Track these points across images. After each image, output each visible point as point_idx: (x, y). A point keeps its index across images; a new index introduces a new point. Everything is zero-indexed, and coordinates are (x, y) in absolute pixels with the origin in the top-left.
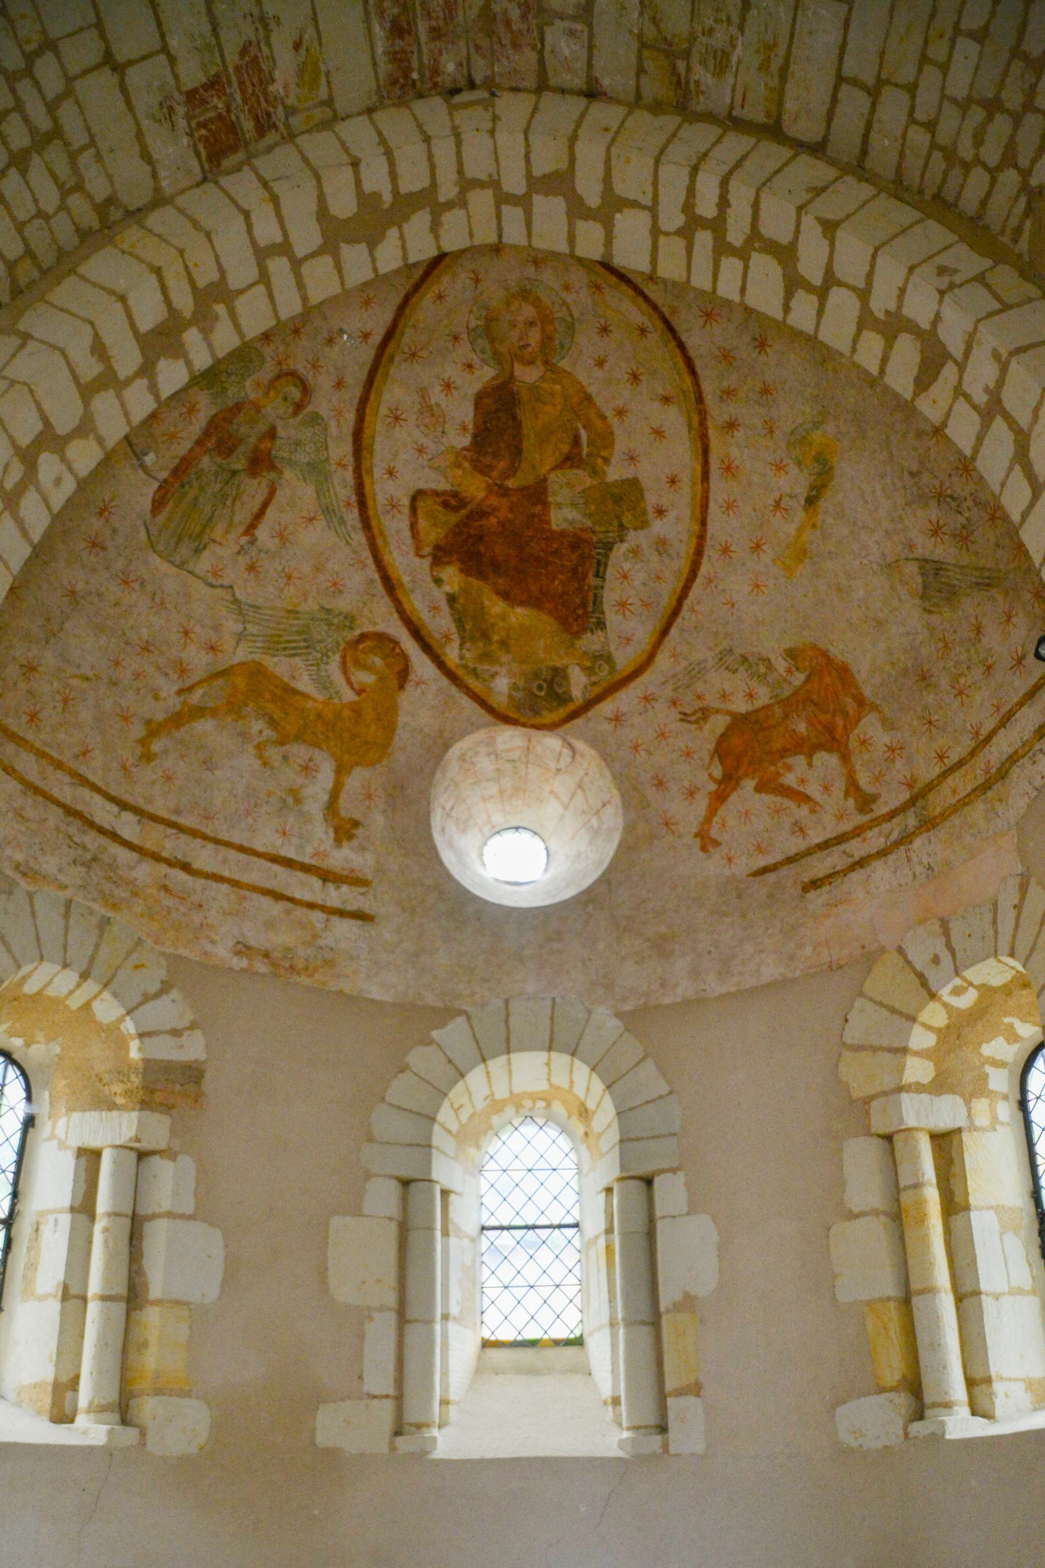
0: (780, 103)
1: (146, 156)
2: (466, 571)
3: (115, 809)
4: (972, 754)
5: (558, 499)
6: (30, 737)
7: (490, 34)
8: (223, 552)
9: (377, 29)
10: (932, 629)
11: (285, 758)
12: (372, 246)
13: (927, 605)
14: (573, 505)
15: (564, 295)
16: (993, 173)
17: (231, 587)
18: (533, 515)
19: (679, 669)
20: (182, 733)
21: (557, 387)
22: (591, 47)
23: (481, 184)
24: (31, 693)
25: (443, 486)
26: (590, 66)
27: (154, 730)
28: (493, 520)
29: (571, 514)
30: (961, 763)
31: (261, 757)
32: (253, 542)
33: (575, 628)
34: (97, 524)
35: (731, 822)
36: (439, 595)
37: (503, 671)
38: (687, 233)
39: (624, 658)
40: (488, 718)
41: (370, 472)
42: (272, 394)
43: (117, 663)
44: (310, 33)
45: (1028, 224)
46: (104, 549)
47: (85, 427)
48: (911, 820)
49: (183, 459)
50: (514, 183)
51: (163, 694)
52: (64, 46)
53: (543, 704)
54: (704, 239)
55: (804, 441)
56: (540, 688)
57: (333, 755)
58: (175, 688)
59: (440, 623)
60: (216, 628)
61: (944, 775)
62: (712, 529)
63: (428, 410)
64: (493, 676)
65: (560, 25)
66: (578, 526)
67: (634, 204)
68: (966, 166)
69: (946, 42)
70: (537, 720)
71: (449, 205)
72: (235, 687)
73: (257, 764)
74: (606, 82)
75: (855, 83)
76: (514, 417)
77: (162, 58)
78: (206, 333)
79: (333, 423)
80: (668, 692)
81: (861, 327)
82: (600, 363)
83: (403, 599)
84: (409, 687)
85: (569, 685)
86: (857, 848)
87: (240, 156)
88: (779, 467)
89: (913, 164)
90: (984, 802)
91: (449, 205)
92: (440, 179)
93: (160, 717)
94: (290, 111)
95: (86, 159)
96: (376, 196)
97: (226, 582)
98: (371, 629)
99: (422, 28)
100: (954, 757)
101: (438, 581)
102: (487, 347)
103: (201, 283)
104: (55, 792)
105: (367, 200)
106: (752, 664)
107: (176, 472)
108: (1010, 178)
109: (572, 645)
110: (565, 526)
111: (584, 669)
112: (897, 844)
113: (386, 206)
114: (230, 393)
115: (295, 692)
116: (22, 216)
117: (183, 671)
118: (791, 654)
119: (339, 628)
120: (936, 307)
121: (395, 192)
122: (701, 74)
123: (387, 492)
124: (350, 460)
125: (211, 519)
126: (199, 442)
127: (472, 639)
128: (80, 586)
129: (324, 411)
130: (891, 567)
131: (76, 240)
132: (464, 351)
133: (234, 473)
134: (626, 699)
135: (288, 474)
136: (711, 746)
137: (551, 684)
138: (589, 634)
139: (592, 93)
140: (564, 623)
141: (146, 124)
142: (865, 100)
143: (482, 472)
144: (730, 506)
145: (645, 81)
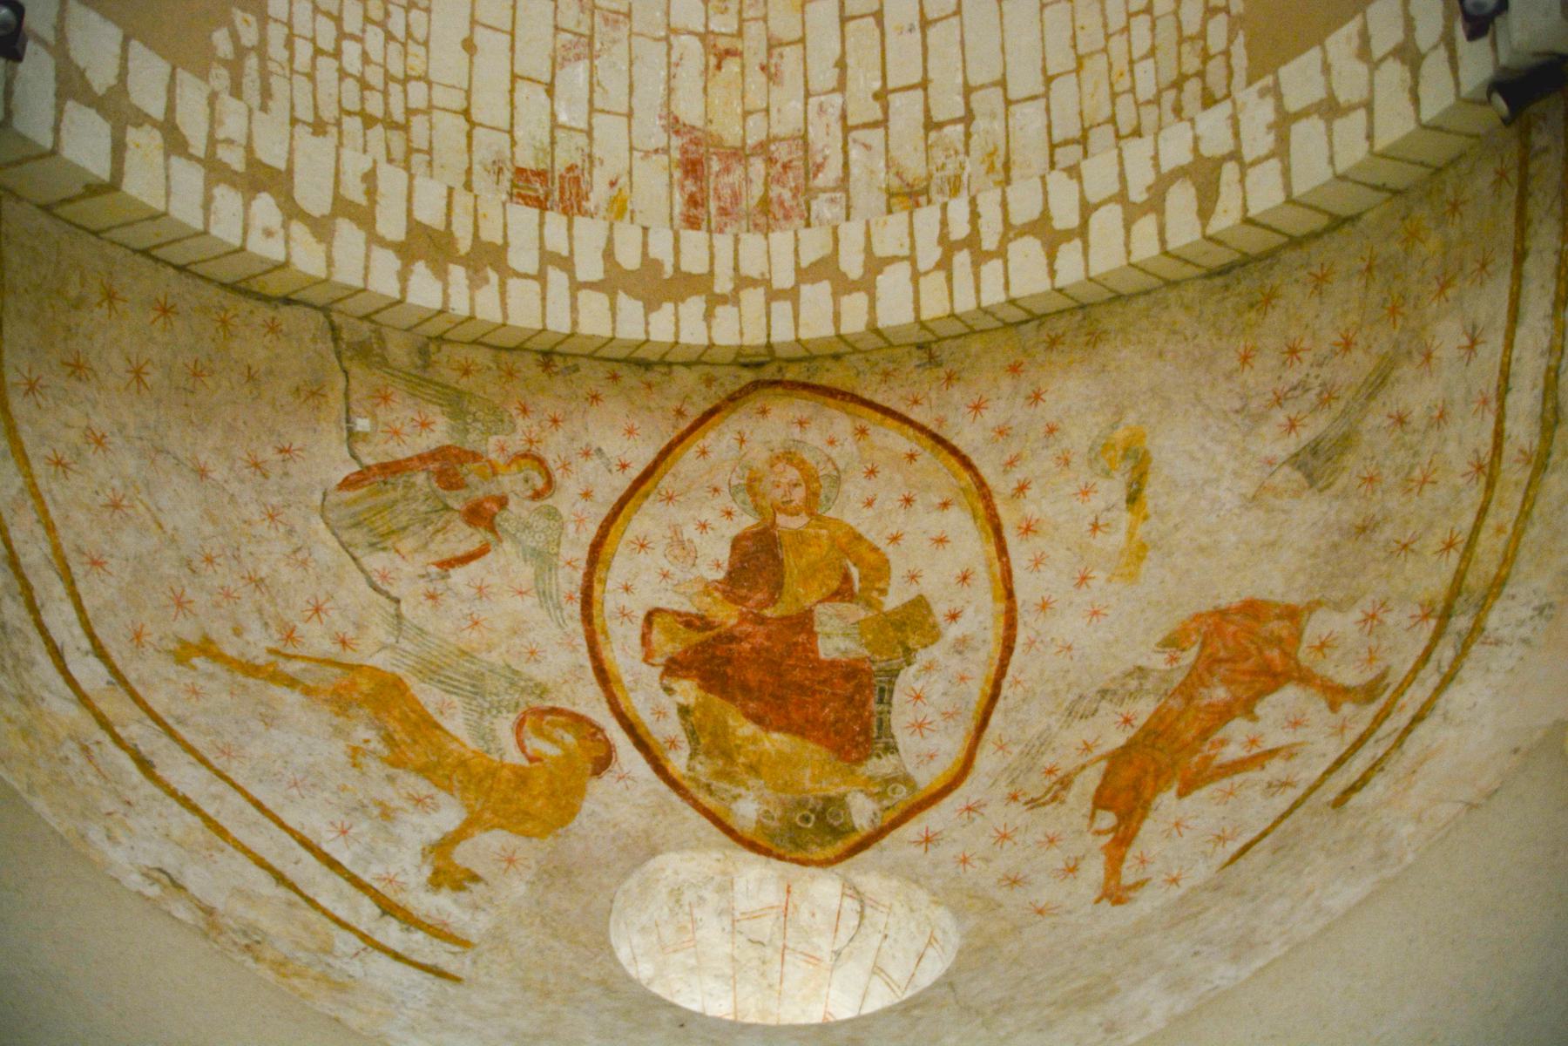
5: (827, 629)
8: (405, 567)
13: (1320, 484)
14: (846, 635)
15: (828, 450)
17: (398, 601)
18: (795, 644)
21: (824, 532)
23: (754, 283)
25: (687, 607)
27: (207, 648)
28: (747, 646)
29: (843, 644)
32: (445, 577)
34: (269, 455)
36: (669, 704)
37: (751, 795)
38: (945, 264)
39: (927, 777)
41: (603, 581)
42: (514, 468)
44: (624, 180)
46: (265, 476)
49: (398, 463)
50: (784, 278)
56: (806, 819)
58: (272, 645)
62: (1020, 596)
63: (679, 545)
64: (735, 798)
65: (823, 196)
66: (852, 656)
69: (1127, 77)
70: (799, 855)
71: (723, 300)
76: (775, 557)
82: (870, 503)
83: (619, 694)
84: (607, 777)
88: (1085, 492)
92: (717, 270)
96: (658, 264)
97: (394, 592)
99: (713, 206)
102: (749, 500)
107: (384, 467)
109: (853, 772)
110: (835, 655)
113: (666, 276)
121: (677, 267)
125: (404, 529)
126: (421, 458)
127: (708, 754)
129: (564, 510)
132: (724, 500)
133: (447, 508)
135: (507, 545)
137: (821, 816)
138: (875, 759)
140: (841, 752)
141: (477, 168)
143: (735, 602)
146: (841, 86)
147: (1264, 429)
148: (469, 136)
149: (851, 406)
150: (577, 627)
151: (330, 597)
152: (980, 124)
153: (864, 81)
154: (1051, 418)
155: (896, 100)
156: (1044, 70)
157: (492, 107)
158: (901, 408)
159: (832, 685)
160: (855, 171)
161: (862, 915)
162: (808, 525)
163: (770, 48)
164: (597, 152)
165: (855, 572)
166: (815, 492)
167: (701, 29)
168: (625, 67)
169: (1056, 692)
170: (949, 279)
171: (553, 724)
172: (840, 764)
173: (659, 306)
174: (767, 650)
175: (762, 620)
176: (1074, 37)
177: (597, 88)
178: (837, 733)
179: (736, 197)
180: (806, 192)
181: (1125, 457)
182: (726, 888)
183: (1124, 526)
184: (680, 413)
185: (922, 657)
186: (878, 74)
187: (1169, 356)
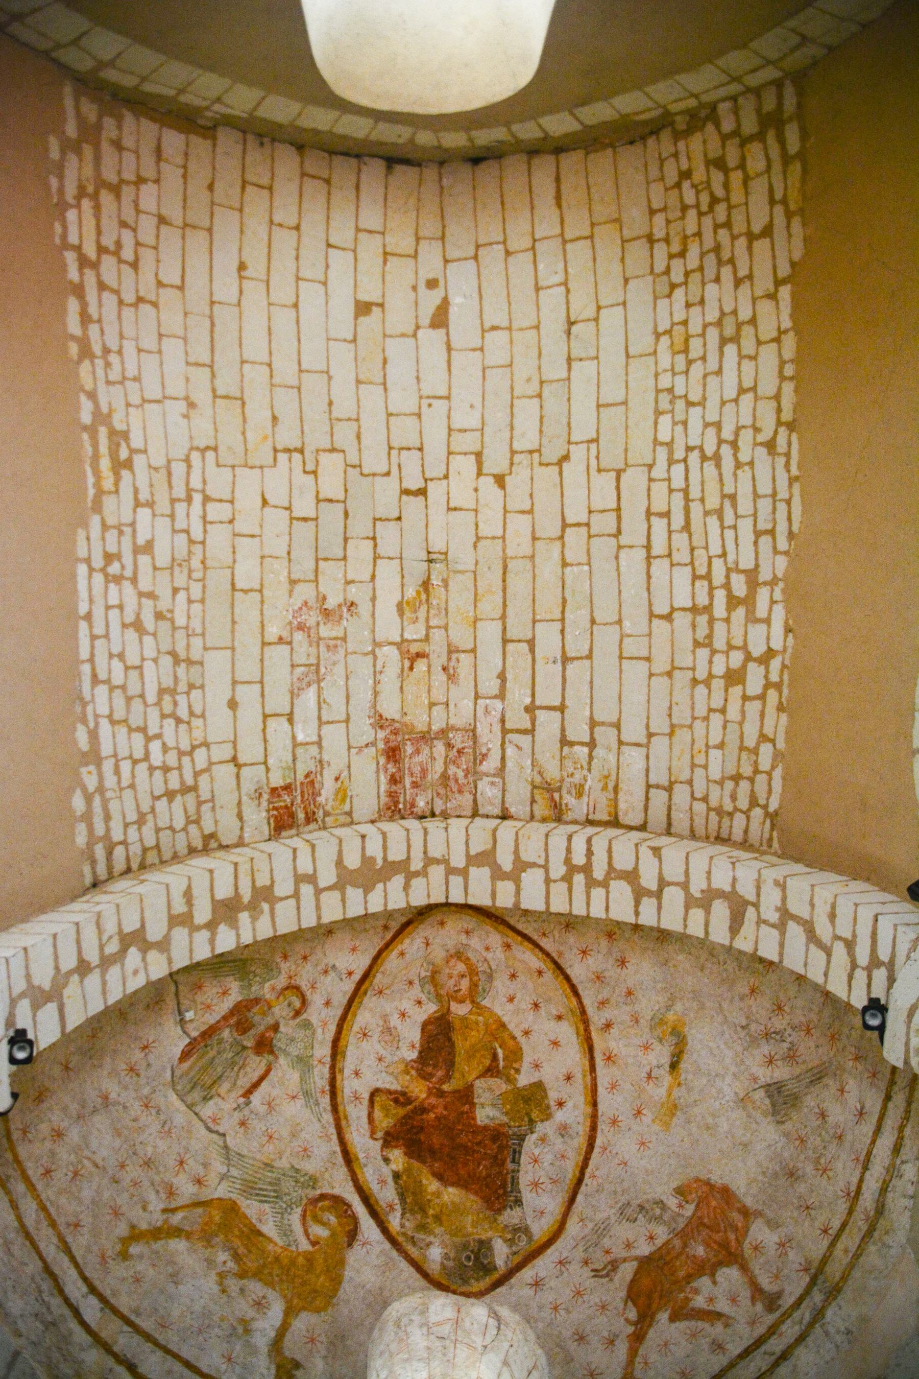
0: (616, 807)
1: (240, 816)
2: (408, 1154)
3: (85, 1289)
4: (850, 1212)
6: (39, 1187)
7: (446, 787)
8: (222, 1107)
9: (382, 777)
10: (787, 1135)
11: (242, 1290)
12: (366, 893)
14: (494, 1105)
15: (485, 954)
16: (747, 813)
17: (224, 1135)
19: (587, 1231)
20: (158, 1245)
22: (504, 791)
23: (437, 861)
24: (53, 1154)
25: (395, 1086)
26: (503, 802)
27: (135, 1235)
28: (432, 1115)
29: (491, 1112)
30: (844, 1225)
31: (221, 1284)
32: (248, 1103)
33: (497, 1206)
34: (138, 1055)
35: (653, 1357)
36: (387, 1172)
37: (436, 1241)
38: (567, 878)
39: (540, 1229)
40: (423, 1283)
41: (342, 1071)
43: (123, 1166)
44: (345, 774)
45: (775, 834)
46: (138, 1075)
47: (163, 945)
48: (817, 1297)
49: (211, 1027)
50: (458, 861)
51: (151, 1208)
52: (213, 747)
53: (471, 1274)
54: (579, 879)
55: (662, 1022)
56: (468, 1258)
57: (285, 1297)
58: (162, 1206)
59: (387, 1195)
60: (206, 1165)
61: (833, 1244)
62: (601, 1108)
65: (486, 780)
67: (534, 865)
68: (731, 815)
69: (703, 754)
71: (417, 874)
72: (211, 1217)
73: (216, 1289)
74: (512, 810)
75: (657, 787)
76: (450, 1039)
77: (263, 767)
78: (254, 919)
79: (319, 1031)
80: (579, 1254)
81: (687, 908)
82: (511, 999)
83: (358, 1171)
84: (357, 1246)
85: (493, 1255)
86: (776, 1345)
87: (294, 832)
88: (646, 1047)
89: (699, 822)
90: (874, 1244)
91: (417, 874)
93: (144, 1226)
94: (327, 814)
95: (205, 808)
96: (373, 859)
98: (330, 1191)
99: (408, 781)
100: (836, 1224)
101: (386, 1160)
103: (259, 884)
104: (42, 1246)
105: (367, 861)
106: (649, 1210)
108: (757, 812)
110: (487, 1121)
111: (506, 1241)
112: (811, 1324)
114: (253, 989)
115: (259, 1233)
116: (161, 824)
117: (171, 1193)
118: (680, 1191)
119: (304, 1186)
120: (731, 874)
121: (385, 859)
122: (569, 799)
123: (354, 1087)
124: (328, 1059)
126: (225, 1018)
127: (412, 1212)
128: (113, 1095)
129: (314, 1020)
130: (743, 1101)
131: (186, 851)
132: (416, 991)
133: (244, 1048)
134: (543, 1265)
135: (282, 1060)
136: (623, 1294)
139: (505, 816)
141: (245, 799)
142: (665, 794)
144: (613, 1086)
145: (535, 806)
146: (501, 695)
147: (755, 1052)
148: (238, 776)
149: (501, 927)
150: (328, 1117)
151: (187, 1150)
152: (599, 752)
153: (519, 696)
154: (630, 983)
155: (541, 715)
156: (647, 727)
157: (250, 751)
158: (535, 937)
159: (485, 1147)
160: (510, 764)
161: (499, 1328)
162: (470, 1012)
163: (450, 652)
164: (326, 757)
165: (501, 1057)
166: (477, 982)
167: (398, 639)
168: (342, 683)
169: (615, 1193)
170: (570, 890)
171: (322, 1209)
172: (488, 1213)
173: (374, 886)
174: (445, 1117)
175: (441, 1094)
176: (670, 708)
177: (324, 706)
178: (487, 1186)
179: (424, 772)
180: (474, 773)
181: (672, 1033)
182: (424, 1312)
183: (666, 1083)
184: (386, 928)
185: (540, 1128)
186: (529, 692)
187: (707, 971)
